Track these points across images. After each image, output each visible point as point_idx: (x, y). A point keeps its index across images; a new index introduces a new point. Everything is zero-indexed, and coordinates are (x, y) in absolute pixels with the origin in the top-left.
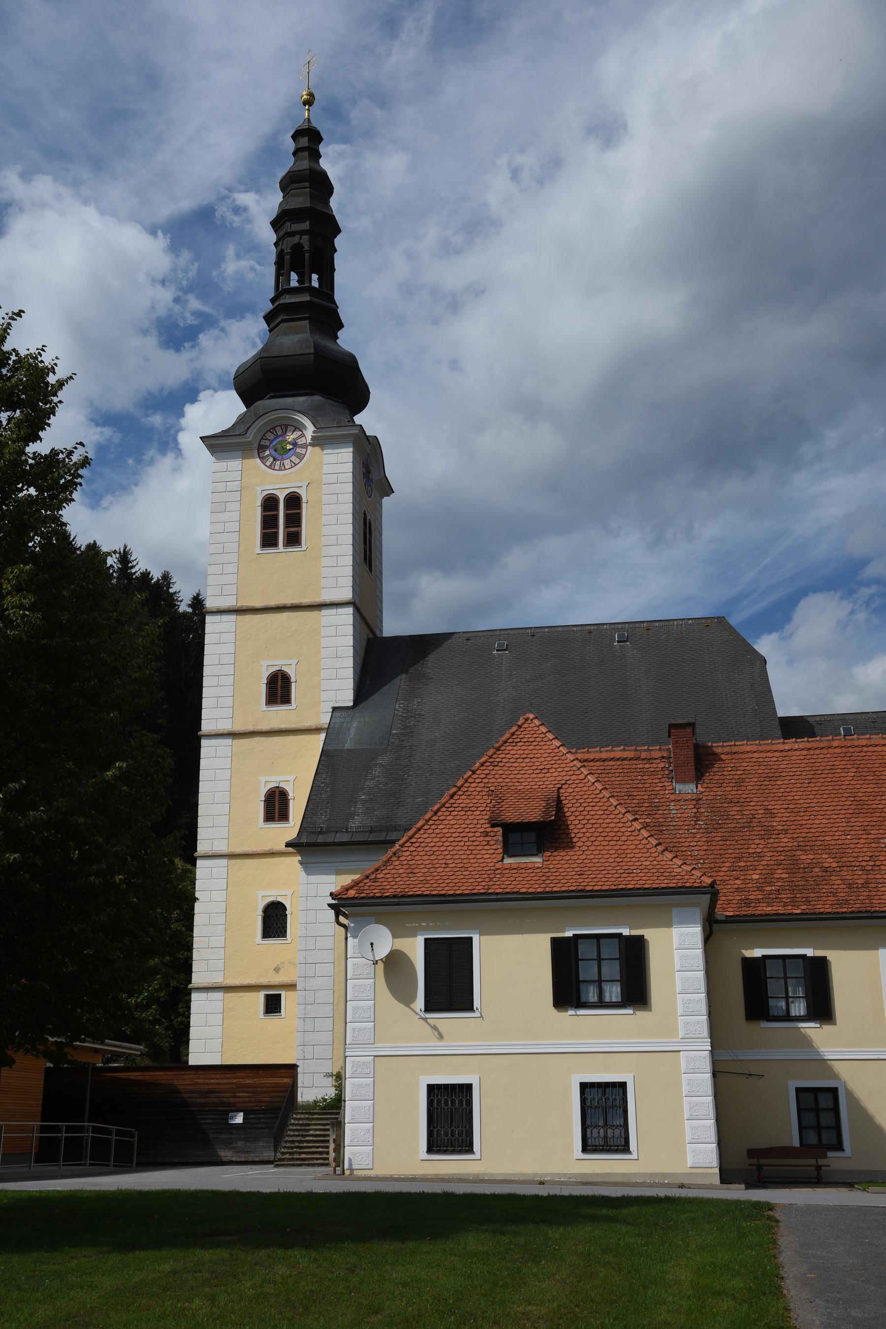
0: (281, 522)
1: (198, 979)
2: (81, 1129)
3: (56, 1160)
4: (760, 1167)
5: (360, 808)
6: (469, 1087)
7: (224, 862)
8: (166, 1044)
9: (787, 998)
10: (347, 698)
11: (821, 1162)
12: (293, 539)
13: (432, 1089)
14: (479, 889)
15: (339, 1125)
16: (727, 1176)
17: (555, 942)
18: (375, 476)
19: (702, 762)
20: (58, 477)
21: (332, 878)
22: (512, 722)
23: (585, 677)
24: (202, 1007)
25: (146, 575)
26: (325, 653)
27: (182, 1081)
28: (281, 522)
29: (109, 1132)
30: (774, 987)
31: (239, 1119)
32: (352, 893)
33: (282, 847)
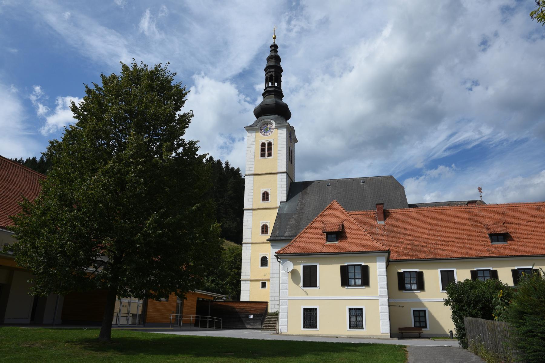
0: (266, 150)
3: (198, 326)
4: (402, 333)
5: (288, 230)
7: (250, 245)
9: (411, 284)
10: (285, 199)
11: (420, 331)
12: (270, 155)
14: (319, 251)
16: (392, 336)
17: (341, 267)
18: (293, 137)
19: (386, 215)
23: (349, 191)
24: (244, 286)
26: (278, 186)
27: (236, 305)
28: (266, 150)
29: (214, 319)
30: (407, 280)
31: (252, 316)
32: (281, 252)
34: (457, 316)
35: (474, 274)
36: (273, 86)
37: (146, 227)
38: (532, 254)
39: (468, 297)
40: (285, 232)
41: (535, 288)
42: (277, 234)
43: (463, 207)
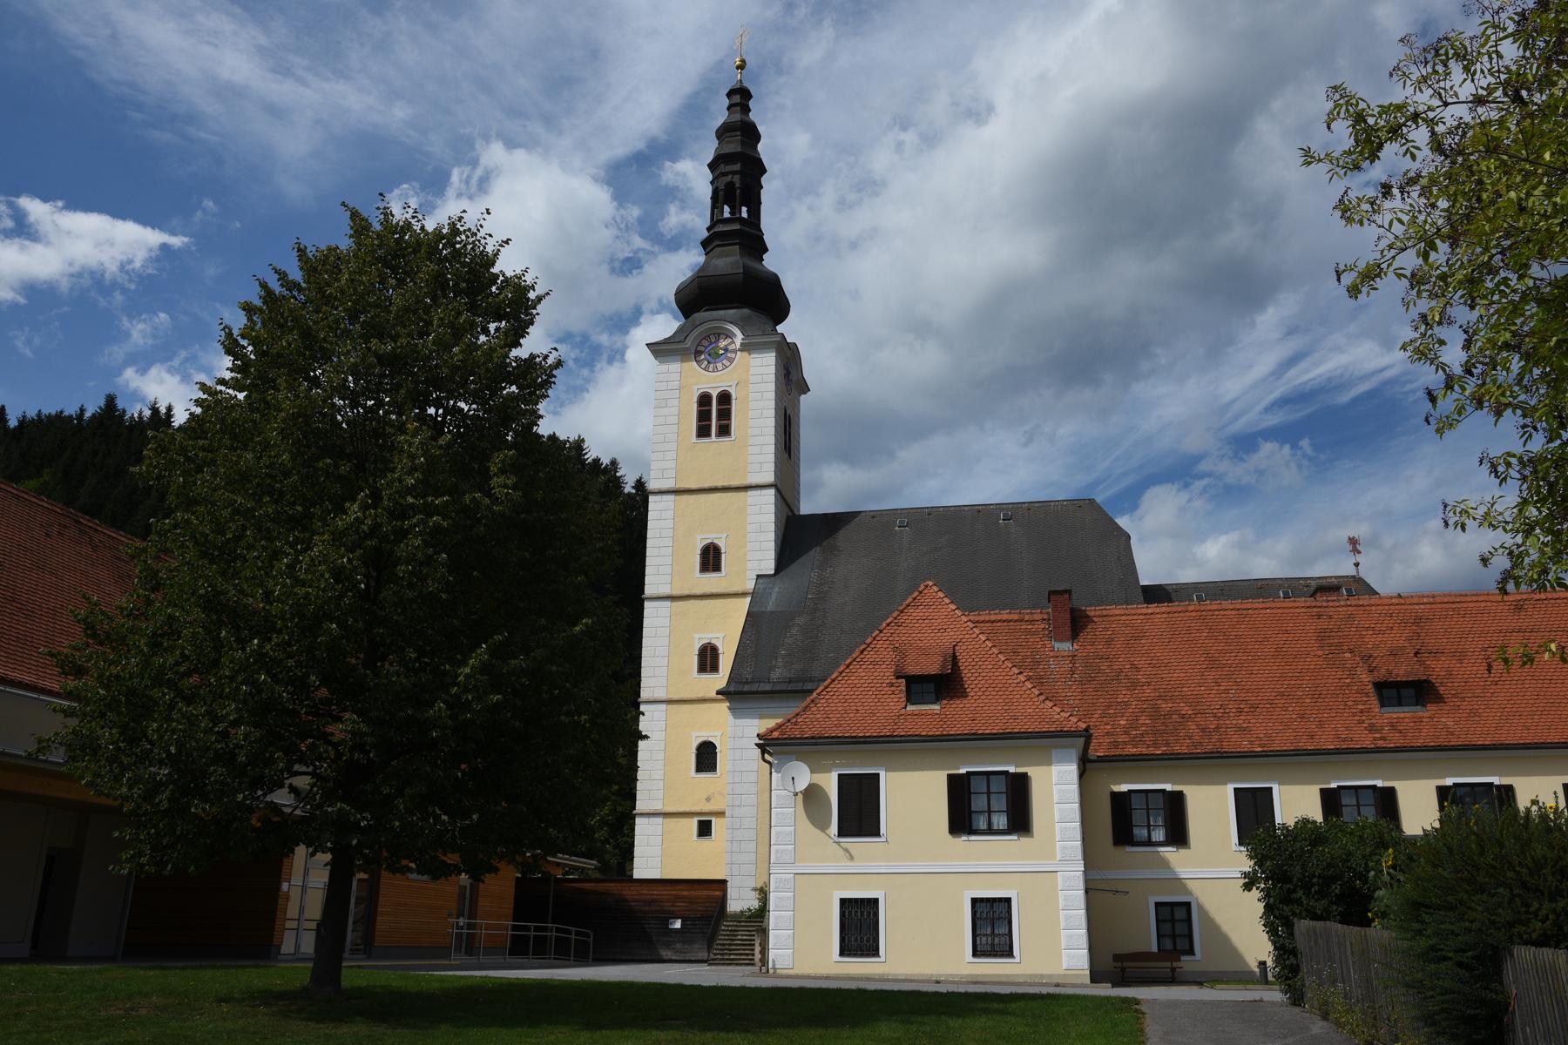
0: (714, 415)
1: (640, 806)
2: (545, 929)
4: (1123, 969)
5: (780, 662)
6: (876, 901)
8: (614, 862)
9: (1149, 826)
10: (769, 567)
11: (1176, 964)
12: (724, 431)
13: (844, 902)
14: (886, 732)
15: (764, 932)
16: (1095, 977)
17: (950, 777)
18: (794, 377)
19: (1077, 624)
20: (536, 378)
21: (756, 722)
22: (914, 587)
23: (968, 548)
24: (647, 836)
25: (597, 461)
26: (750, 528)
27: (629, 892)
28: (714, 415)
29: (569, 932)
30: (1138, 816)
31: (678, 925)
32: (775, 734)
33: (713, 694)
34: (1277, 919)
35: (1330, 799)
36: (735, 218)
37: (458, 684)
38: (1496, 740)
39: (1304, 867)
40: (772, 668)
41: (1450, 849)
42: (747, 674)
43: (1302, 601)
